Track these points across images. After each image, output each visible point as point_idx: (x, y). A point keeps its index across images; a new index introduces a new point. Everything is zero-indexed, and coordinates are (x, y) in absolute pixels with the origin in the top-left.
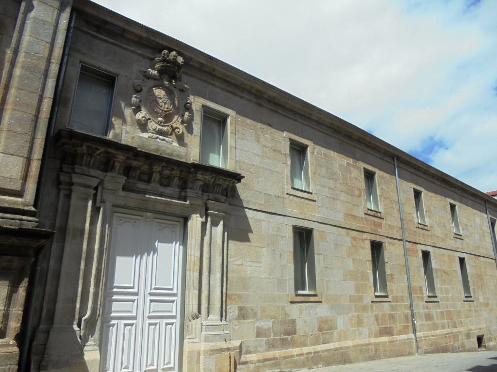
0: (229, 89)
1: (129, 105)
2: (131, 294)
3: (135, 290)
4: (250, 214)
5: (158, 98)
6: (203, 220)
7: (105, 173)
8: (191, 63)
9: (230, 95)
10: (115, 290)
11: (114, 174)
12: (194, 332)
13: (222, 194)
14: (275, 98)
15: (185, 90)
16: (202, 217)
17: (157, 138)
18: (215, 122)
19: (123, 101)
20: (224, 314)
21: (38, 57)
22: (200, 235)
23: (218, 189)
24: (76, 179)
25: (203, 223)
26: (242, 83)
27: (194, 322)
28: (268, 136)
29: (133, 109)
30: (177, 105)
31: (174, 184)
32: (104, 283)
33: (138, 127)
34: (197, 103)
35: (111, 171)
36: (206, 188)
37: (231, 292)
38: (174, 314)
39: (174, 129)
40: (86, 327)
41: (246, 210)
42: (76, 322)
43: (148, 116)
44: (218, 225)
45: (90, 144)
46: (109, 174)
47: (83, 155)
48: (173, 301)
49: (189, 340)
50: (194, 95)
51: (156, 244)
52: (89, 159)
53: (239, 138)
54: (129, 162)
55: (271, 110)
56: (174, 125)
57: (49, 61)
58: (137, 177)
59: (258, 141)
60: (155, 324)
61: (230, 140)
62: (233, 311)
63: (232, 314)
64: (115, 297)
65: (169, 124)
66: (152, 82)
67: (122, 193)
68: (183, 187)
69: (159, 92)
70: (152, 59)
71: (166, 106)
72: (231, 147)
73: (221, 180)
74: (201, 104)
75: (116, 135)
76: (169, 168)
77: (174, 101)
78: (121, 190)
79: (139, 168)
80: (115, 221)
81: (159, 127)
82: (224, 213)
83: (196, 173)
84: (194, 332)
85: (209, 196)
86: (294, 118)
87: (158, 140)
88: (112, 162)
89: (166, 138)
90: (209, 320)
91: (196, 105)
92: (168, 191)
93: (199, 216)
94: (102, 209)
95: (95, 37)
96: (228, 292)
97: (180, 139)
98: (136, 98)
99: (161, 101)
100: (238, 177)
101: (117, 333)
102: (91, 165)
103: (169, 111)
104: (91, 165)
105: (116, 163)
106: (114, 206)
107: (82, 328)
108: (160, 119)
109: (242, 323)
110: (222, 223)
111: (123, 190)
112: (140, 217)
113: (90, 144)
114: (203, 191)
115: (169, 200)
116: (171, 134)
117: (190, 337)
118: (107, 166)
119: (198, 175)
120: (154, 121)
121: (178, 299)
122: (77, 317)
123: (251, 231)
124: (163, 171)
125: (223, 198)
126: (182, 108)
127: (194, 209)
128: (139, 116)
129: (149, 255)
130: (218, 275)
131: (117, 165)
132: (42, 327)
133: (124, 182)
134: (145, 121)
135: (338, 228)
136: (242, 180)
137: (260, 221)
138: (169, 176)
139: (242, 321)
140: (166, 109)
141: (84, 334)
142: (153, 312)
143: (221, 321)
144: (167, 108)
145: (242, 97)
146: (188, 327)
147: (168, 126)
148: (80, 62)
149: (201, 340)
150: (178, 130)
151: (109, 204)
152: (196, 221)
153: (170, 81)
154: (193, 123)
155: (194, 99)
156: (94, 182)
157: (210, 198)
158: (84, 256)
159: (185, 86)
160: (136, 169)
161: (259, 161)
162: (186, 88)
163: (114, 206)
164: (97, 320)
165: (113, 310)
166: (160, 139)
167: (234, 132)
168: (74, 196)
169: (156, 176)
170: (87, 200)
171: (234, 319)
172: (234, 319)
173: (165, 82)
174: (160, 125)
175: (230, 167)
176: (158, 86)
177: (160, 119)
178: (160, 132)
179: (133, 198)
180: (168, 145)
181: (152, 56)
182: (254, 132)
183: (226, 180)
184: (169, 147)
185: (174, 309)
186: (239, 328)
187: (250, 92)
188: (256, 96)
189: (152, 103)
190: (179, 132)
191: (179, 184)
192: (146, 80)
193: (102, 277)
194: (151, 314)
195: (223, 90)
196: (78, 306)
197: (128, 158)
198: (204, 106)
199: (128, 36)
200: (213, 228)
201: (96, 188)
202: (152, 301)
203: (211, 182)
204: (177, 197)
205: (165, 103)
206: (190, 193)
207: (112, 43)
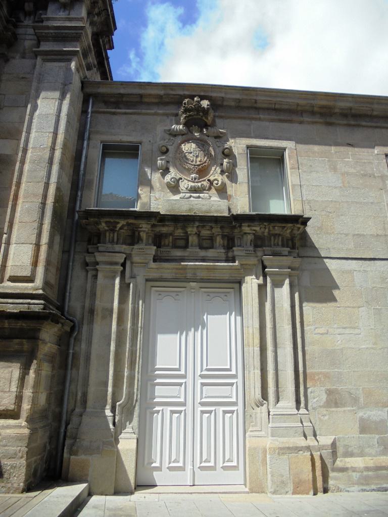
0: (282, 117)
1: (155, 168)
2: (177, 376)
3: (182, 372)
4: (331, 265)
5: (187, 154)
6: (261, 281)
7: (132, 247)
8: (225, 103)
9: (285, 125)
10: (157, 372)
11: (142, 246)
12: (259, 424)
13: (283, 246)
14: (351, 109)
15: (221, 135)
16: (258, 278)
17: (191, 196)
18: (269, 163)
19: (148, 167)
20: (302, 399)
21: (42, 148)
22: (256, 300)
23: (276, 241)
24: (99, 258)
25: (260, 286)
26: (298, 105)
27: (258, 410)
28: (351, 160)
29: (161, 173)
30: (213, 153)
31: (218, 244)
32: (140, 367)
33: (169, 191)
34: (238, 145)
35: (138, 242)
36: (259, 242)
37: (314, 371)
38: (234, 400)
39: (211, 182)
40: (122, 413)
41: (325, 260)
42: (108, 407)
43: (179, 176)
44: (283, 285)
45: (107, 220)
46: (136, 247)
47: (106, 231)
48: (232, 384)
49: (252, 433)
50: (232, 137)
51: (205, 317)
52: (112, 235)
53: (305, 172)
54: (158, 229)
55: (349, 125)
56: (212, 178)
57: (53, 149)
58: (171, 244)
59: (334, 169)
60: (210, 412)
61: (291, 176)
62: (317, 394)
63: (315, 400)
64: (158, 381)
65: (205, 178)
66: (179, 139)
67: (153, 265)
68: (230, 244)
69: (189, 148)
70: (177, 115)
71: (199, 159)
72: (293, 186)
73: (276, 228)
74: (245, 146)
75: (143, 205)
76: (208, 228)
77: (208, 150)
78: (152, 261)
79: (171, 234)
80: (154, 296)
81: (193, 184)
82: (289, 269)
83: (240, 226)
84: (259, 424)
85: (264, 251)
86: (258, 116)
87: (192, 199)
88: (137, 233)
89: (201, 195)
90: (278, 408)
91: (238, 148)
92: (211, 253)
93: (255, 278)
94: (131, 285)
95: (114, 113)
96: (308, 371)
97: (222, 191)
98: (161, 160)
99: (191, 155)
100: (300, 221)
101: (163, 423)
102: (115, 240)
103: (202, 164)
104: (115, 240)
105: (141, 234)
106: (147, 280)
107: (117, 413)
108: (193, 175)
109: (333, 411)
110: (287, 282)
111: (154, 262)
112: (183, 289)
113: (107, 220)
114: (256, 246)
115: (211, 264)
116: (210, 189)
117: (254, 429)
118: (133, 239)
119: (243, 228)
120: (187, 180)
121: (240, 380)
122: (109, 401)
123: (337, 287)
124: (200, 232)
125: (286, 250)
126: (220, 156)
127: (247, 270)
128: (168, 178)
129: (196, 330)
130: (288, 349)
131: (143, 235)
132: (77, 410)
133: (154, 253)
134: (174, 182)
135: (329, 256)
136: (309, 223)
137: (350, 272)
138: (211, 237)
139: (333, 409)
140: (198, 163)
141: (120, 420)
142: (205, 397)
143: (298, 408)
144: (200, 161)
145: (301, 123)
146: (251, 416)
147: (205, 180)
148: (101, 143)
149: (268, 434)
150: (216, 182)
151: (140, 280)
152: (251, 284)
153: (201, 131)
154: (237, 169)
155: (235, 142)
156: (120, 258)
157: (266, 253)
158: (113, 336)
159: (220, 130)
160: (166, 236)
161: (339, 194)
162: (221, 133)
163: (147, 280)
164: (135, 405)
165: (156, 394)
166: (194, 197)
167: (296, 166)
168: (100, 275)
169: (193, 239)
170: (114, 279)
171: (320, 407)
172: (320, 407)
173: (196, 134)
174: (194, 182)
175: (295, 210)
176: (187, 141)
177: (193, 175)
178: (194, 190)
179: (168, 269)
180: (204, 202)
181: (175, 112)
182: (327, 159)
183: (284, 227)
184: (211, 204)
185: (233, 394)
186: (329, 418)
187: (313, 113)
188: (322, 115)
189: (181, 161)
190: (217, 184)
191: (223, 243)
192: (172, 138)
193: (138, 358)
194: (204, 400)
195: (272, 121)
196: (110, 389)
197: (153, 226)
198: (248, 147)
199: (146, 100)
200: (277, 290)
201: (124, 265)
202: (203, 384)
203: (266, 234)
204: (224, 259)
205: (197, 157)
206: (237, 251)
207: (131, 114)
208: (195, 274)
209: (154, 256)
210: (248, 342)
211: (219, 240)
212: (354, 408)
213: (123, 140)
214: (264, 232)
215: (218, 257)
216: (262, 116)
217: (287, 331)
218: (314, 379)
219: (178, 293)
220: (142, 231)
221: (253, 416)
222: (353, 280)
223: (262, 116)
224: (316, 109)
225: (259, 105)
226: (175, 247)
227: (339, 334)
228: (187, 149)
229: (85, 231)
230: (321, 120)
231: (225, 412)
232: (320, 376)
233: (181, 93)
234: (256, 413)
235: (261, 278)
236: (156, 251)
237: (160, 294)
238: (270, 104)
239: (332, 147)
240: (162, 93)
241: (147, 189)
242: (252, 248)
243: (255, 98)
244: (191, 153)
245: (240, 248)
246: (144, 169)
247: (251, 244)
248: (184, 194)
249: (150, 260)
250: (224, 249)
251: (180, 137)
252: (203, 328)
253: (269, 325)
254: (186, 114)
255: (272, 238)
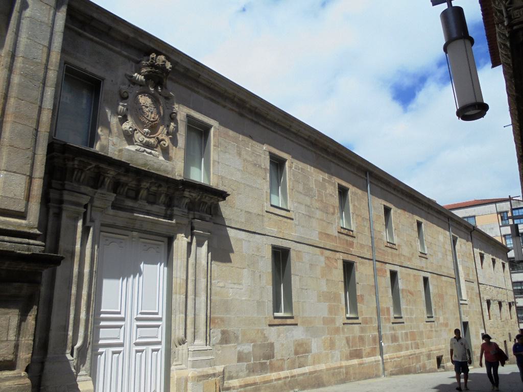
1: (116, 113)
4: (231, 233)
7: (96, 190)
10: (102, 316)
14: (256, 108)
17: (144, 151)
23: (203, 207)
26: (226, 91)
28: (250, 150)
29: (119, 118)
31: (160, 201)
33: (124, 139)
34: (182, 112)
41: (228, 229)
42: (68, 351)
44: (203, 245)
45: (82, 159)
46: (99, 191)
52: (79, 174)
53: (222, 151)
59: (239, 154)
64: (102, 323)
66: (137, 89)
67: (111, 212)
68: (169, 205)
69: (144, 100)
71: (153, 116)
72: (214, 161)
75: (103, 147)
76: (157, 185)
78: (110, 208)
83: (184, 191)
87: (145, 153)
88: (102, 178)
89: (153, 152)
92: (155, 208)
95: (80, 35)
97: (165, 152)
98: (123, 106)
99: (147, 109)
108: (146, 130)
110: (206, 243)
113: (82, 159)
114: (189, 209)
116: (157, 147)
118: (97, 182)
121: (163, 324)
123: (232, 251)
126: (167, 118)
127: (179, 229)
131: (107, 181)
137: (241, 240)
138: (155, 193)
139: (224, 345)
140: (152, 120)
142: (139, 338)
144: (153, 118)
145: (224, 107)
148: (65, 64)
151: (97, 223)
152: (181, 241)
153: (156, 88)
154: (178, 134)
155: (179, 108)
160: (124, 185)
162: (171, 96)
169: (143, 193)
170: (77, 220)
171: (217, 344)
175: (214, 183)
177: (146, 130)
178: (147, 145)
179: (122, 217)
186: (221, 353)
189: (137, 112)
193: (92, 302)
194: (138, 341)
195: (206, 97)
201: (86, 206)
202: (138, 327)
205: (152, 113)
208: (142, 225)
209: (113, 203)
210: (176, 290)
211: (162, 198)
212: (236, 344)
213: (87, 69)
214: (195, 198)
215: (159, 212)
216: (201, 91)
217: (203, 283)
218: (214, 323)
219: (122, 241)
220: (107, 176)
221: (177, 353)
222: (242, 247)
223: (201, 91)
224: (236, 99)
225: (200, 80)
226: (128, 197)
227: (231, 288)
228: (143, 101)
229: (71, 172)
230: (237, 110)
231: (114, 353)
232: (218, 320)
233: (152, 46)
234: (179, 350)
235: (190, 237)
236: (116, 199)
237: (145, 246)
238: (208, 82)
239: (241, 136)
240: (132, 35)
241: (106, 131)
242: (186, 211)
243: (200, 73)
244: (147, 107)
245: (179, 209)
246: (105, 109)
247: (186, 207)
248: (139, 147)
249: (109, 206)
250: (165, 206)
251: (138, 87)
252: (140, 276)
253: (191, 278)
254: (151, 69)
255: (202, 204)
